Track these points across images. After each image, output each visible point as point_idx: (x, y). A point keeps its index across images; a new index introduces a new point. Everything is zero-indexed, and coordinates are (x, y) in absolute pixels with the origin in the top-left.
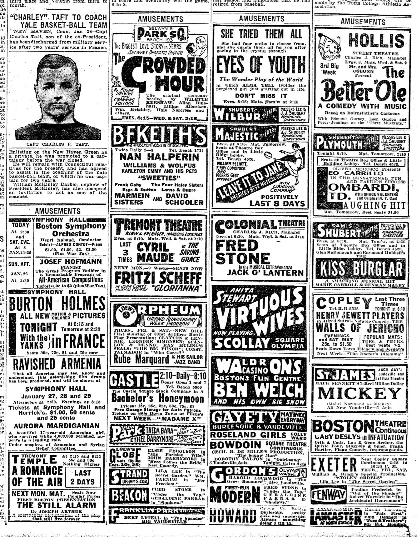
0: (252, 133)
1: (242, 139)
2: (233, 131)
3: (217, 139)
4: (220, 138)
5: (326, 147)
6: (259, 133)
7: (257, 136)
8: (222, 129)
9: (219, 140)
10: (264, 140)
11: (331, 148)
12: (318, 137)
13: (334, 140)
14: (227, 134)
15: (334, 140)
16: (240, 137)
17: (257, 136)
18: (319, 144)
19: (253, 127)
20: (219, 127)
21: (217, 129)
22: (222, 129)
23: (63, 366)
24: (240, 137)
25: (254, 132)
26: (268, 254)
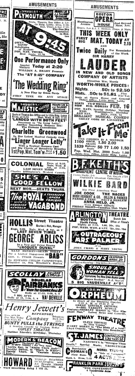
0: (34, 107)
1: (28, 110)
2: (23, 106)
3: (13, 110)
4: (14, 109)
5: (20, 17)
6: (39, 107)
7: (37, 109)
8: (16, 104)
9: (14, 111)
10: (41, 111)
11: (23, 17)
12: (16, 11)
13: (25, 13)
14: (19, 107)
15: (25, 13)
16: (26, 109)
17: (37, 109)
18: (16, 15)
19: (35, 103)
20: (14, 103)
21: (13, 104)
22: (16, 104)
23: (41, 240)
24: (26, 109)
25: (35, 106)
26: (125, 320)
